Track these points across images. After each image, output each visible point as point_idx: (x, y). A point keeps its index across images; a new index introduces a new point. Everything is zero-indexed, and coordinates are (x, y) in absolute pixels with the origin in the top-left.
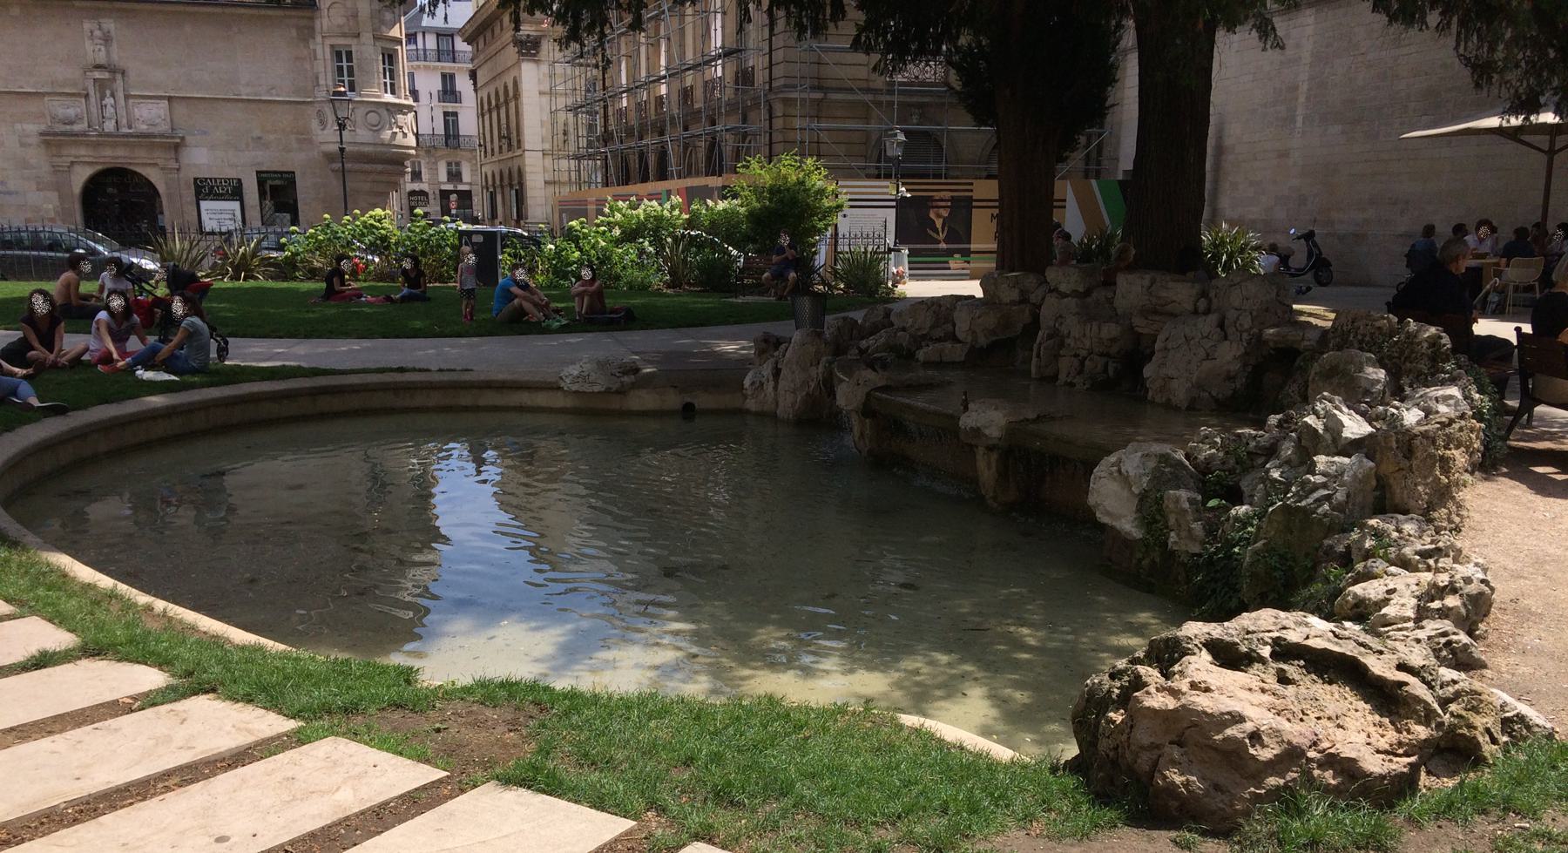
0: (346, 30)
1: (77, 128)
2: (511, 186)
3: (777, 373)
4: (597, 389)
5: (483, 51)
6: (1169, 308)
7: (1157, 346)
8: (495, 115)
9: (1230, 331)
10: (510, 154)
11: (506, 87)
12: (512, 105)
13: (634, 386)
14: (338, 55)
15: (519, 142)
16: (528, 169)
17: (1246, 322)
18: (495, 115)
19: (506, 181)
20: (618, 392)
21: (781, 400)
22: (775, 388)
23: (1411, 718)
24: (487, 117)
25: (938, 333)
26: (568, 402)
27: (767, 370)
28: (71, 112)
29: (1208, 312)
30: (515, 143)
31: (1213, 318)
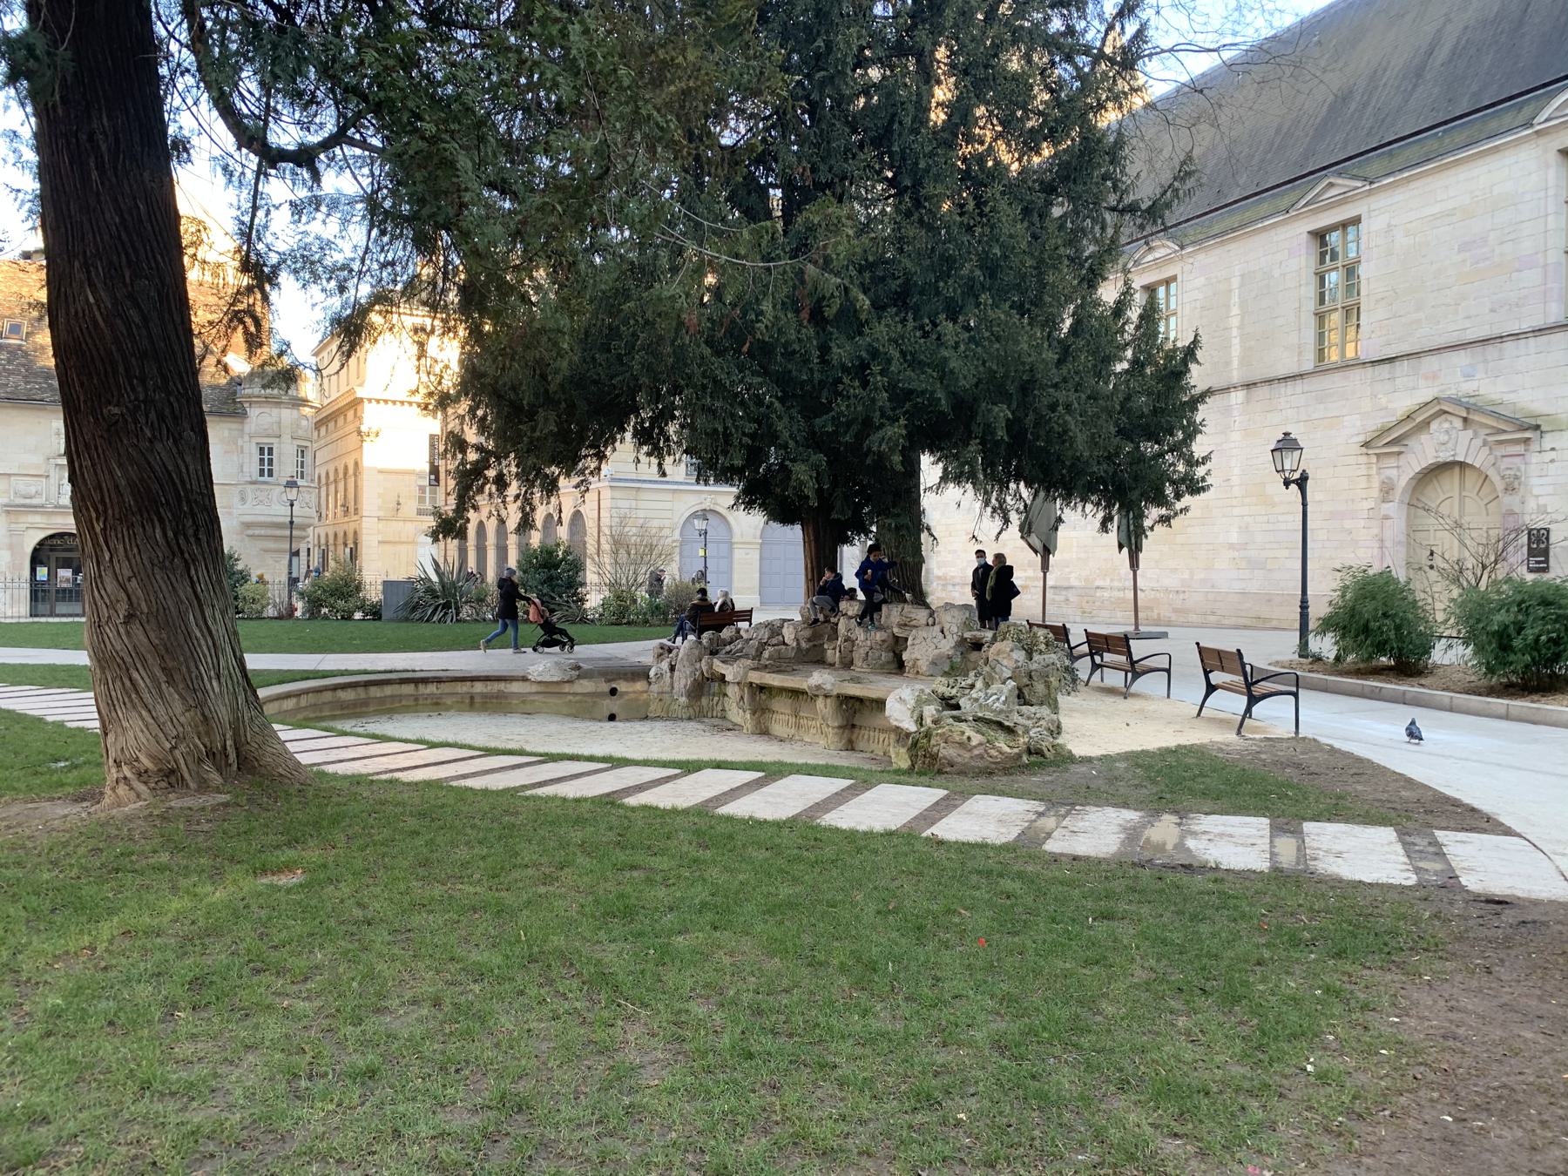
0: (270, 432)
1: (35, 501)
2: (346, 545)
3: (672, 668)
4: (555, 679)
5: (324, 437)
6: (914, 623)
7: (909, 642)
8: (332, 488)
9: (946, 633)
10: (346, 519)
11: (346, 468)
12: (351, 481)
13: (579, 677)
14: (262, 450)
15: (356, 509)
16: (364, 531)
17: (955, 629)
18: (332, 488)
19: (340, 540)
20: (568, 682)
21: (676, 685)
22: (672, 677)
23: (1110, 251)
24: (324, 489)
25: (774, 641)
26: (534, 688)
27: (665, 665)
28: (33, 490)
29: (934, 624)
30: (352, 510)
31: (937, 628)
